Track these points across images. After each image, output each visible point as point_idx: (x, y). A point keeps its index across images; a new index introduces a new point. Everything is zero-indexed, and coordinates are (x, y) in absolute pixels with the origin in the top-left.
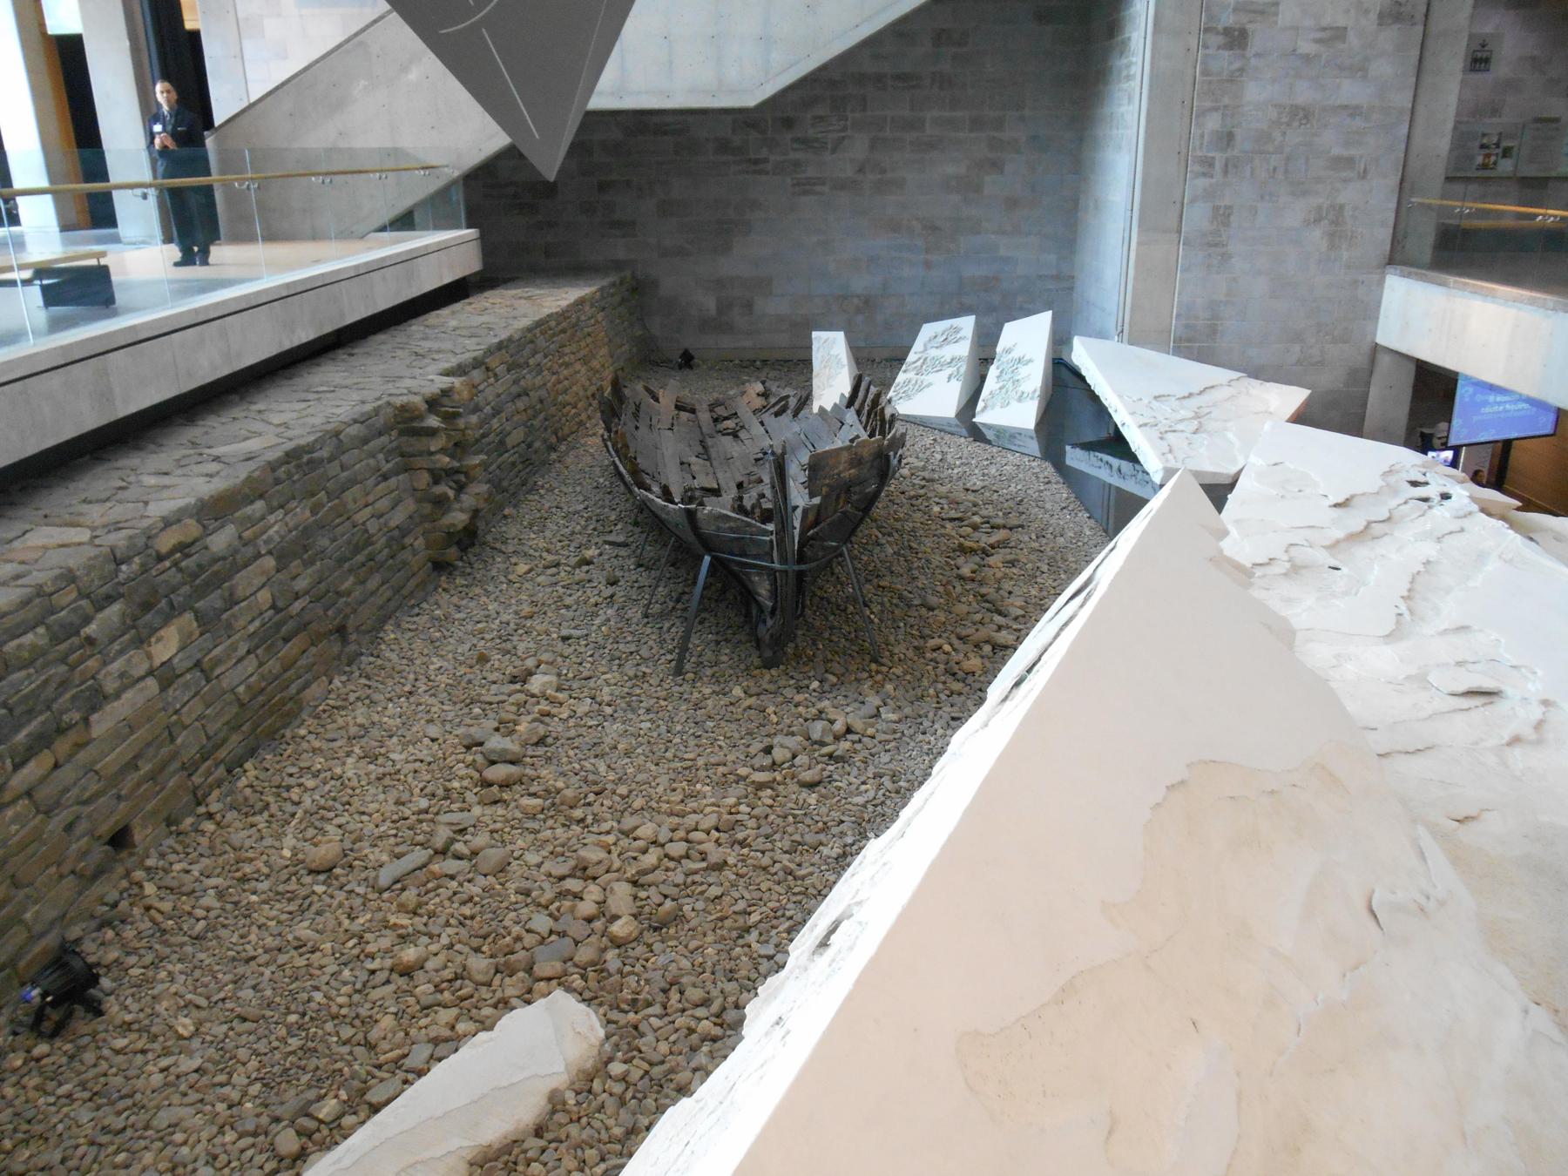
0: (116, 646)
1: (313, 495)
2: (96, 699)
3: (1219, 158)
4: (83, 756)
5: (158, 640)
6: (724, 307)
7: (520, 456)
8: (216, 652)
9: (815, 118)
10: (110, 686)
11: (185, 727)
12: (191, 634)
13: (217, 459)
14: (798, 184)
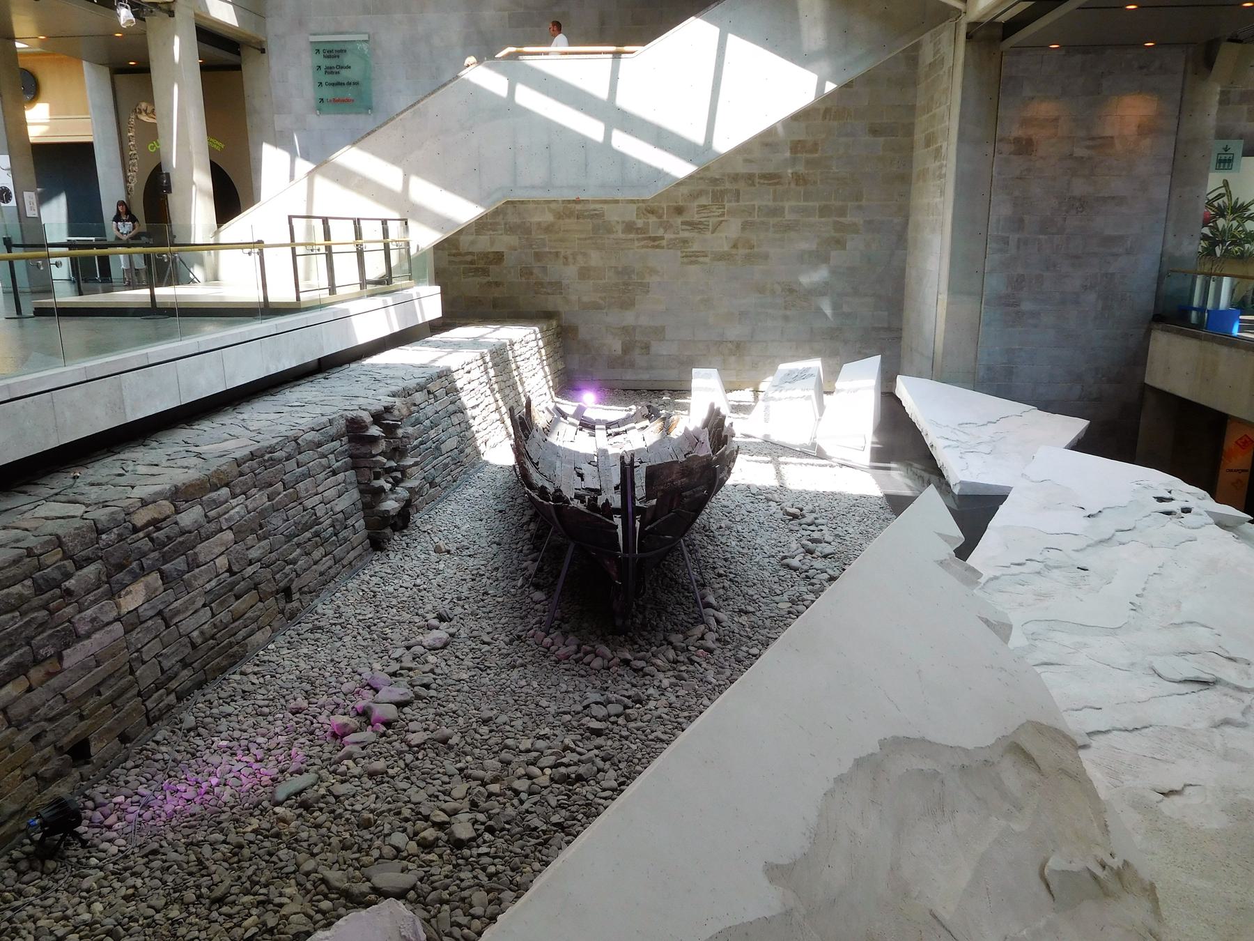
0: (91, 597)
1: (271, 485)
2: (72, 637)
3: (1014, 237)
4: (55, 682)
5: (127, 594)
6: (626, 350)
7: (453, 459)
8: (176, 604)
9: (699, 206)
10: (82, 629)
11: (144, 663)
12: (156, 589)
13: (198, 455)
14: (686, 256)
